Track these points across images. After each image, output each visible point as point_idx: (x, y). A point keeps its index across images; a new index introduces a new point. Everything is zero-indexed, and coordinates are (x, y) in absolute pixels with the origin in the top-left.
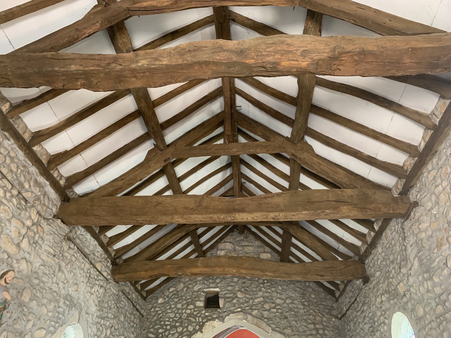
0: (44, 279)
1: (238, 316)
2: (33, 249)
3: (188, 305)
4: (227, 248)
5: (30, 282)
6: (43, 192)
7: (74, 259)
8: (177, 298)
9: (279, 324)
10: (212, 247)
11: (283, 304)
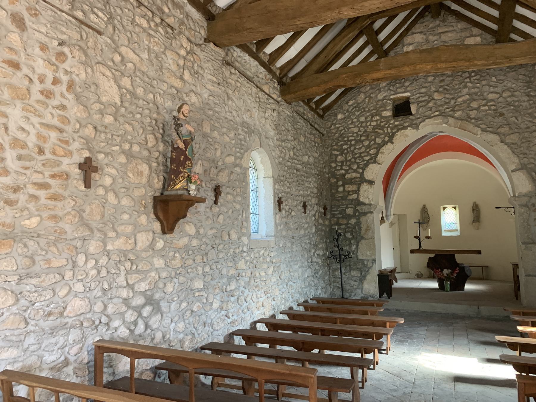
0: (216, 109)
1: (435, 120)
2: (196, 79)
3: (373, 117)
4: (416, 41)
5: (205, 114)
6: (185, 14)
7: (239, 85)
8: (358, 111)
9: (492, 123)
10: (395, 44)
11: (498, 99)
